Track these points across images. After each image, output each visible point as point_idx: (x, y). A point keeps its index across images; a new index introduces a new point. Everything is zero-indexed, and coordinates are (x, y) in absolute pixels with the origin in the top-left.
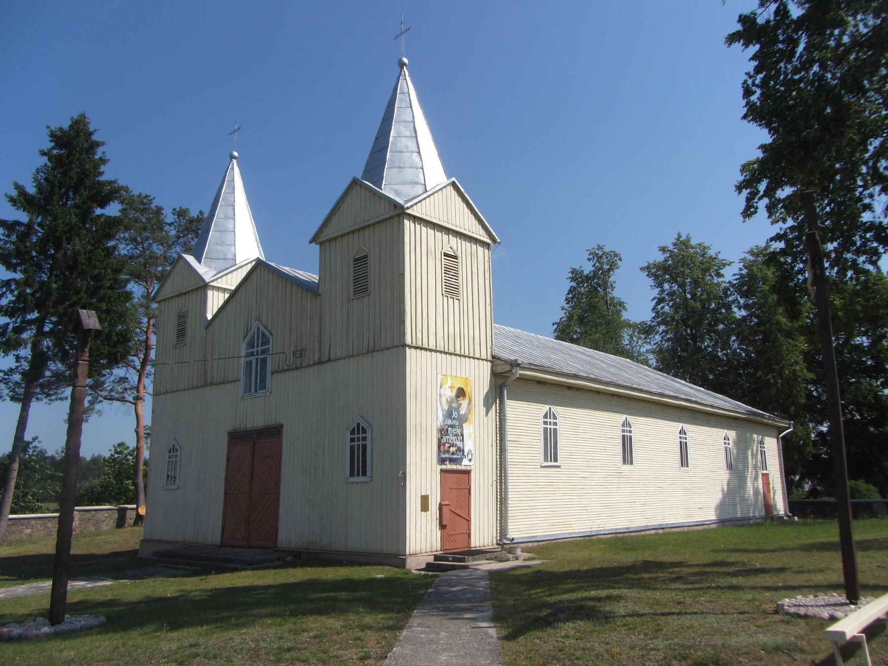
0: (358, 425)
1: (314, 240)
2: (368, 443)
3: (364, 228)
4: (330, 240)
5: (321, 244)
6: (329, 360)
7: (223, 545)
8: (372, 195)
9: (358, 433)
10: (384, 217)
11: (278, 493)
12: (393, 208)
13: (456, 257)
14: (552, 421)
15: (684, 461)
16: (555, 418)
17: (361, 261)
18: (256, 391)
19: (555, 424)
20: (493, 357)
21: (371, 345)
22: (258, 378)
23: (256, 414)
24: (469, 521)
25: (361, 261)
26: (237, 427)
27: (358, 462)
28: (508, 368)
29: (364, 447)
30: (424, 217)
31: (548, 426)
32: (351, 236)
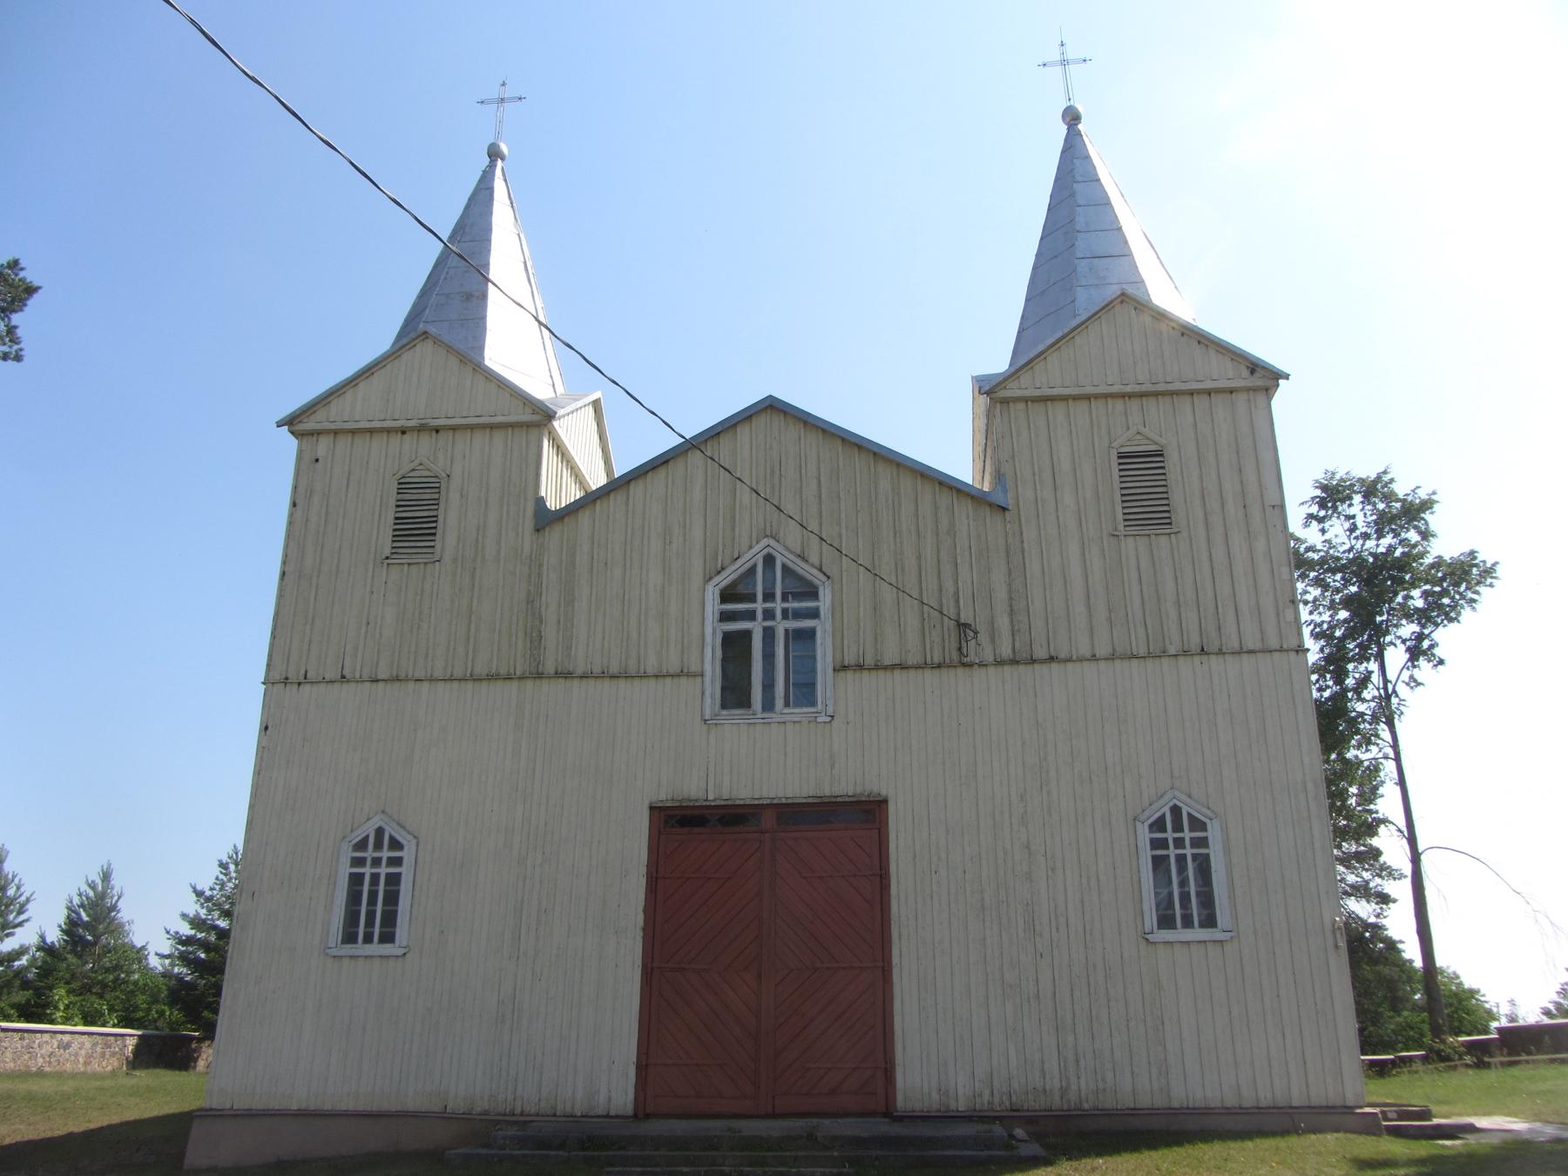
2: (405, 871)
18: (787, 704)
23: (765, 760)
29: (394, 880)
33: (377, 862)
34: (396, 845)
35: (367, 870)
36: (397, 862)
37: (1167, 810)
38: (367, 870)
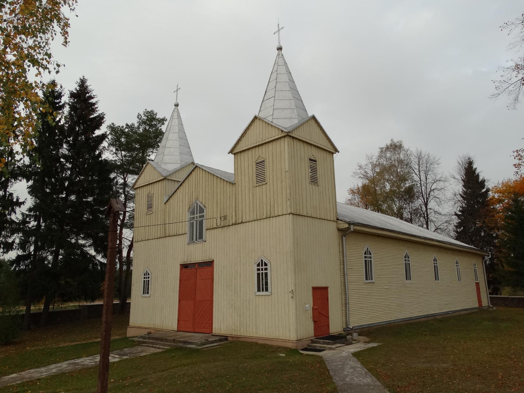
0: (262, 261)
1: (231, 152)
2: (268, 271)
3: (262, 145)
4: (241, 152)
5: (235, 154)
6: (242, 223)
7: (178, 331)
8: (267, 125)
9: (262, 266)
10: (275, 138)
11: (212, 301)
12: (280, 132)
13: (315, 161)
14: (369, 256)
15: (437, 278)
16: (370, 254)
17: (260, 164)
18: (196, 240)
19: (365, 257)
20: (337, 219)
21: (268, 213)
22: (197, 233)
23: (197, 254)
24: (328, 317)
25: (260, 164)
26: (185, 260)
27: (262, 282)
28: (346, 226)
29: (266, 274)
30: (299, 138)
31: (367, 259)
32: (254, 150)
33: (262, 270)
34: (266, 265)
35: (261, 272)
36: (266, 269)
37: (260, 261)
38: (261, 272)
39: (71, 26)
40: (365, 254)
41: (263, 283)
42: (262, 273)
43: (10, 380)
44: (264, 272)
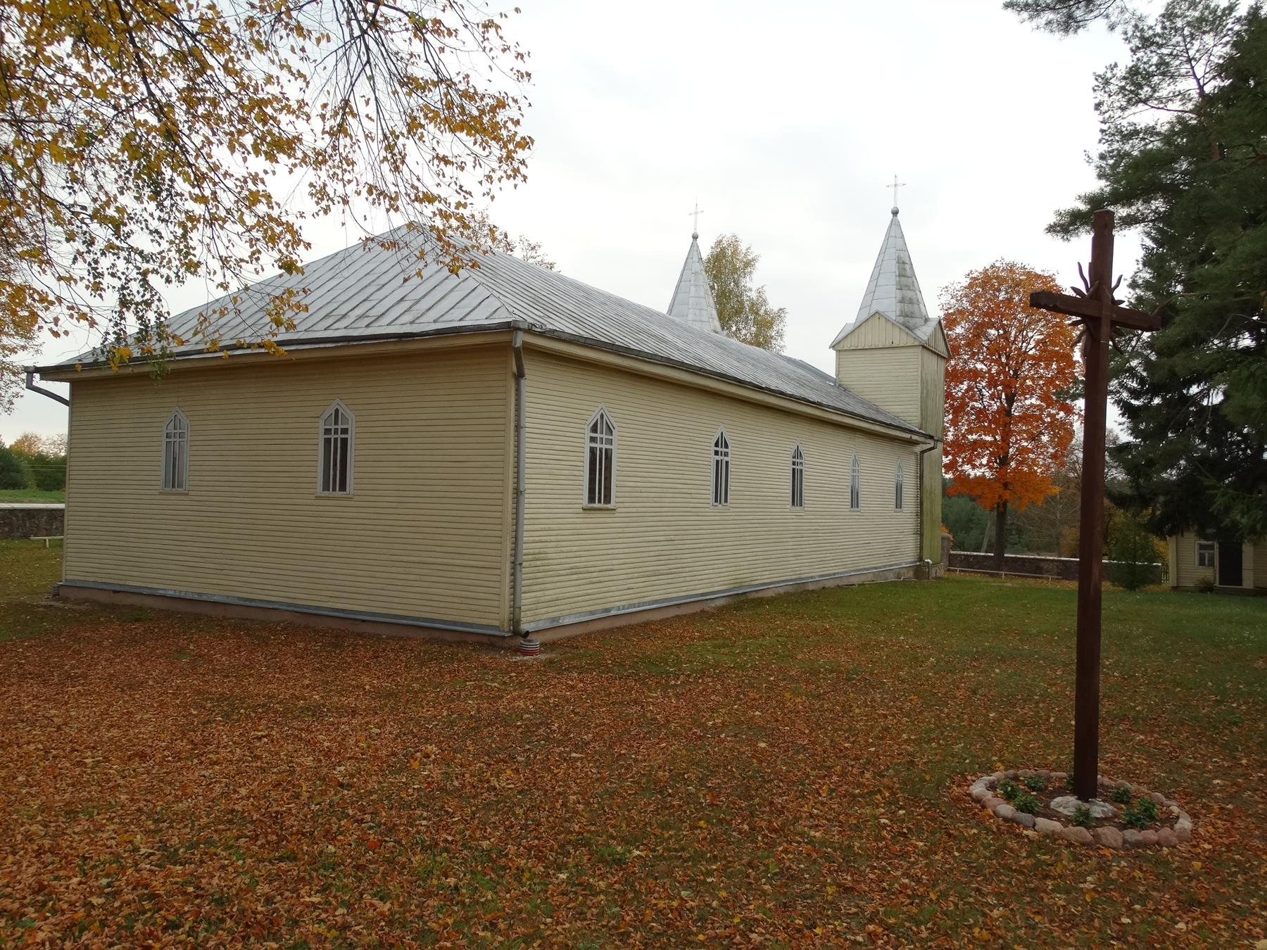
1: (833, 347)
5: (839, 351)
16: (726, 446)
19: (593, 440)
31: (598, 446)
35: (333, 436)
38: (333, 436)
39: (728, 234)
40: (717, 445)
41: (855, 501)
42: (336, 440)
43: (520, 339)
44: (340, 436)
